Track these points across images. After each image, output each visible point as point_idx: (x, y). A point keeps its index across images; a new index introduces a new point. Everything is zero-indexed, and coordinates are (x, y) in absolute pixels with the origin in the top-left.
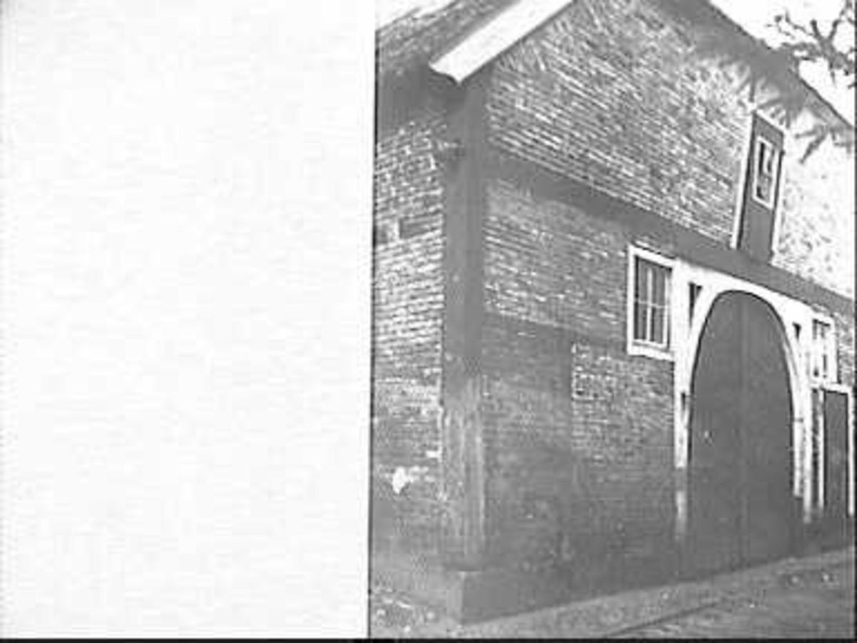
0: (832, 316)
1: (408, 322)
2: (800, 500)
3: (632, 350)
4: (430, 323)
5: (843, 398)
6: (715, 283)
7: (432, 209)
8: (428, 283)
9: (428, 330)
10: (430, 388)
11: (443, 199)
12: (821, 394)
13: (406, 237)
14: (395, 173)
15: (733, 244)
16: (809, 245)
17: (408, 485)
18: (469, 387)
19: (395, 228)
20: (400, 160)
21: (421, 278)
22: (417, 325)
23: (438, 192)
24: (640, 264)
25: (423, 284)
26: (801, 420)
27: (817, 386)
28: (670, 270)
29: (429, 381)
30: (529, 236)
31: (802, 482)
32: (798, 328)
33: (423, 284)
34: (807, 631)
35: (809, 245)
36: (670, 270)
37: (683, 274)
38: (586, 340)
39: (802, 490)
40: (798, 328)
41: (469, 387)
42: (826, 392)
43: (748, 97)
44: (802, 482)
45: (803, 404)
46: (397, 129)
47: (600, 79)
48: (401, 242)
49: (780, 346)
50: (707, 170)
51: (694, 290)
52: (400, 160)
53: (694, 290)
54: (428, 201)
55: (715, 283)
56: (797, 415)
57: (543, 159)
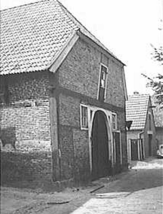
2: (111, 161)
3: (82, 128)
5: (118, 135)
7: (46, 100)
9: (47, 129)
12: (114, 134)
13: (38, 106)
15: (98, 99)
20: (34, 87)
24: (83, 108)
26: (110, 140)
29: (47, 140)
31: (111, 156)
34: (152, 190)
37: (89, 108)
38: (74, 127)
39: (111, 158)
40: (109, 117)
42: (116, 133)
45: (111, 136)
46: (33, 79)
47: (76, 66)
48: (36, 107)
49: (105, 121)
51: (91, 112)
52: (34, 87)
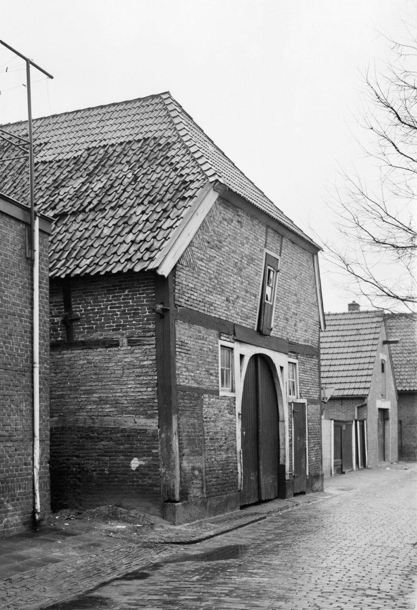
0: (297, 358)
1: (136, 388)
2: (284, 466)
4: (149, 389)
6: (249, 351)
8: (147, 370)
10: (152, 420)
11: (155, 330)
12: (292, 404)
14: (123, 312)
16: (287, 320)
17: (140, 466)
18: (273, 477)
19: (125, 340)
21: (143, 367)
22: (142, 390)
23: (151, 326)
25: (144, 370)
27: (291, 401)
28: (232, 349)
30: (188, 345)
32: (282, 368)
33: (144, 370)
35: (287, 320)
36: (232, 349)
37: (239, 349)
39: (285, 461)
40: (282, 368)
41: (273, 477)
42: (295, 403)
43: (377, 340)
44: (285, 456)
45: (285, 412)
50: (247, 292)
53: (242, 356)
54: (146, 330)
55: (249, 351)
56: (281, 419)
57: (191, 305)
